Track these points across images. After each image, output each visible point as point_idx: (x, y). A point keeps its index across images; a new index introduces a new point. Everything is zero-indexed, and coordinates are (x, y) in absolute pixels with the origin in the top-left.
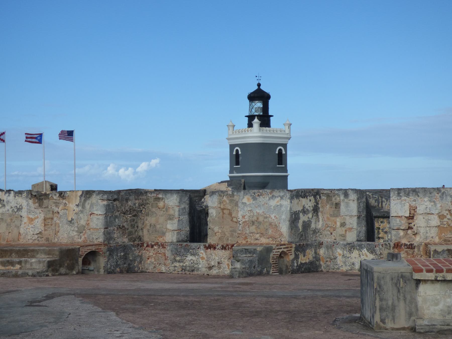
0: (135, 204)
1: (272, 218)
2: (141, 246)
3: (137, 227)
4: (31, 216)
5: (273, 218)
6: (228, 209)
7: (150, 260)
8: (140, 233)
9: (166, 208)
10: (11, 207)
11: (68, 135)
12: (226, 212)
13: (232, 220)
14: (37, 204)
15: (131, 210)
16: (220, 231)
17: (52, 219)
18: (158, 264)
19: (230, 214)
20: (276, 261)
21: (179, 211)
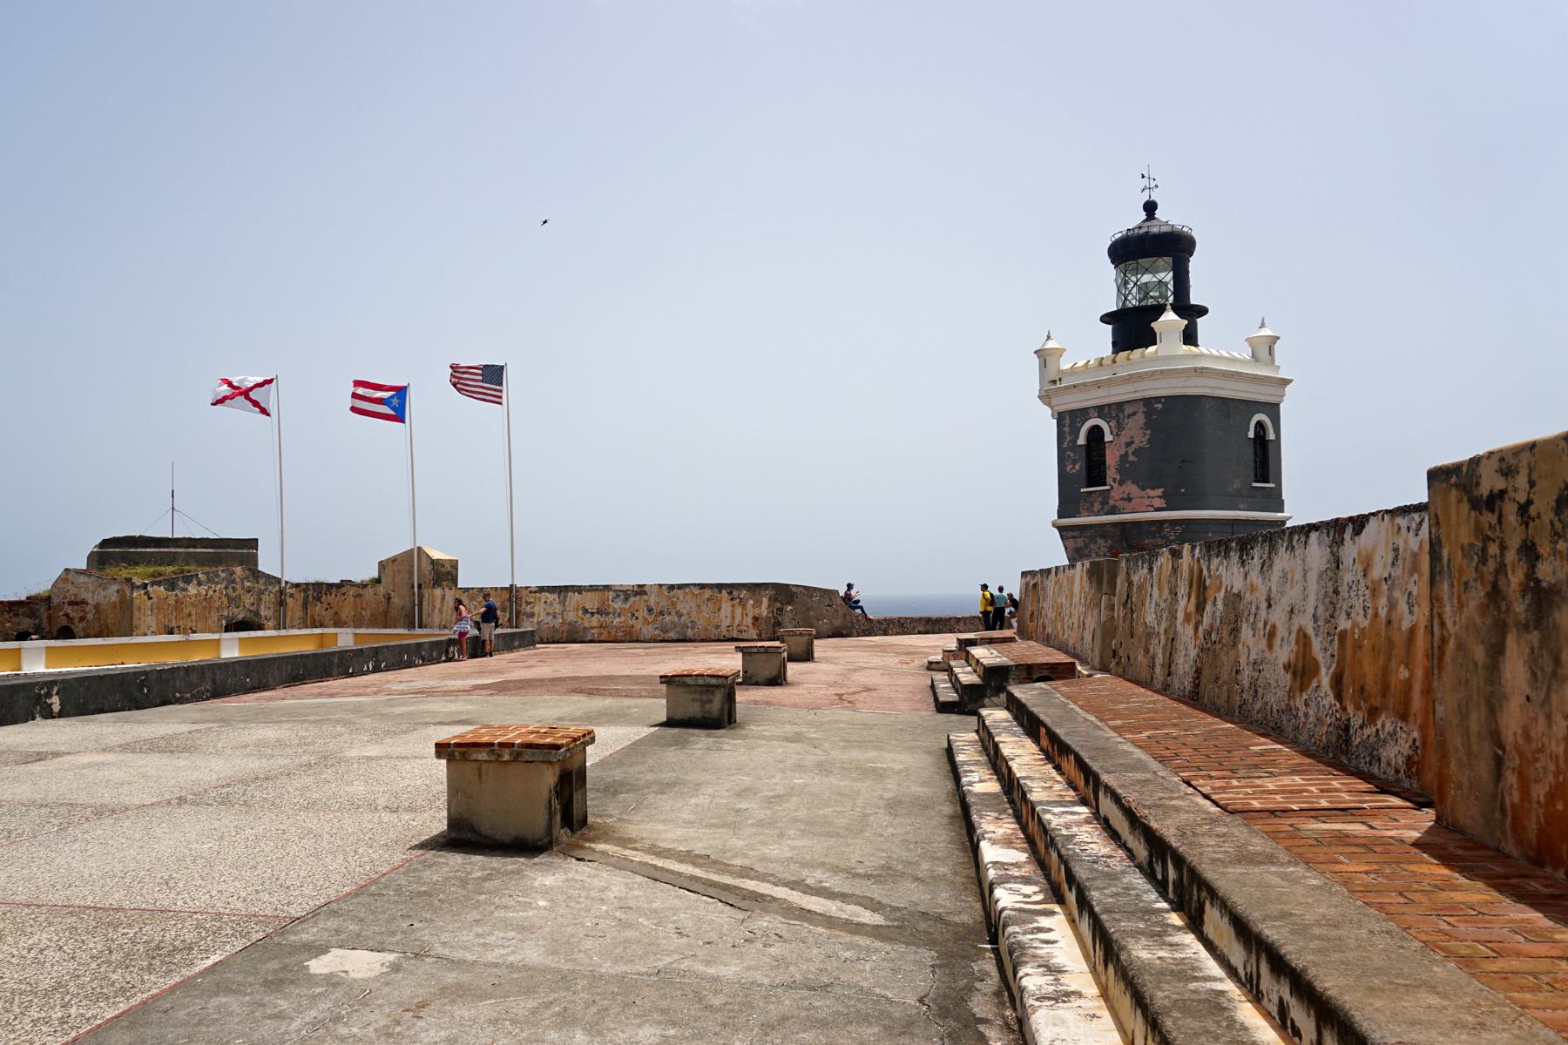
11: (485, 381)
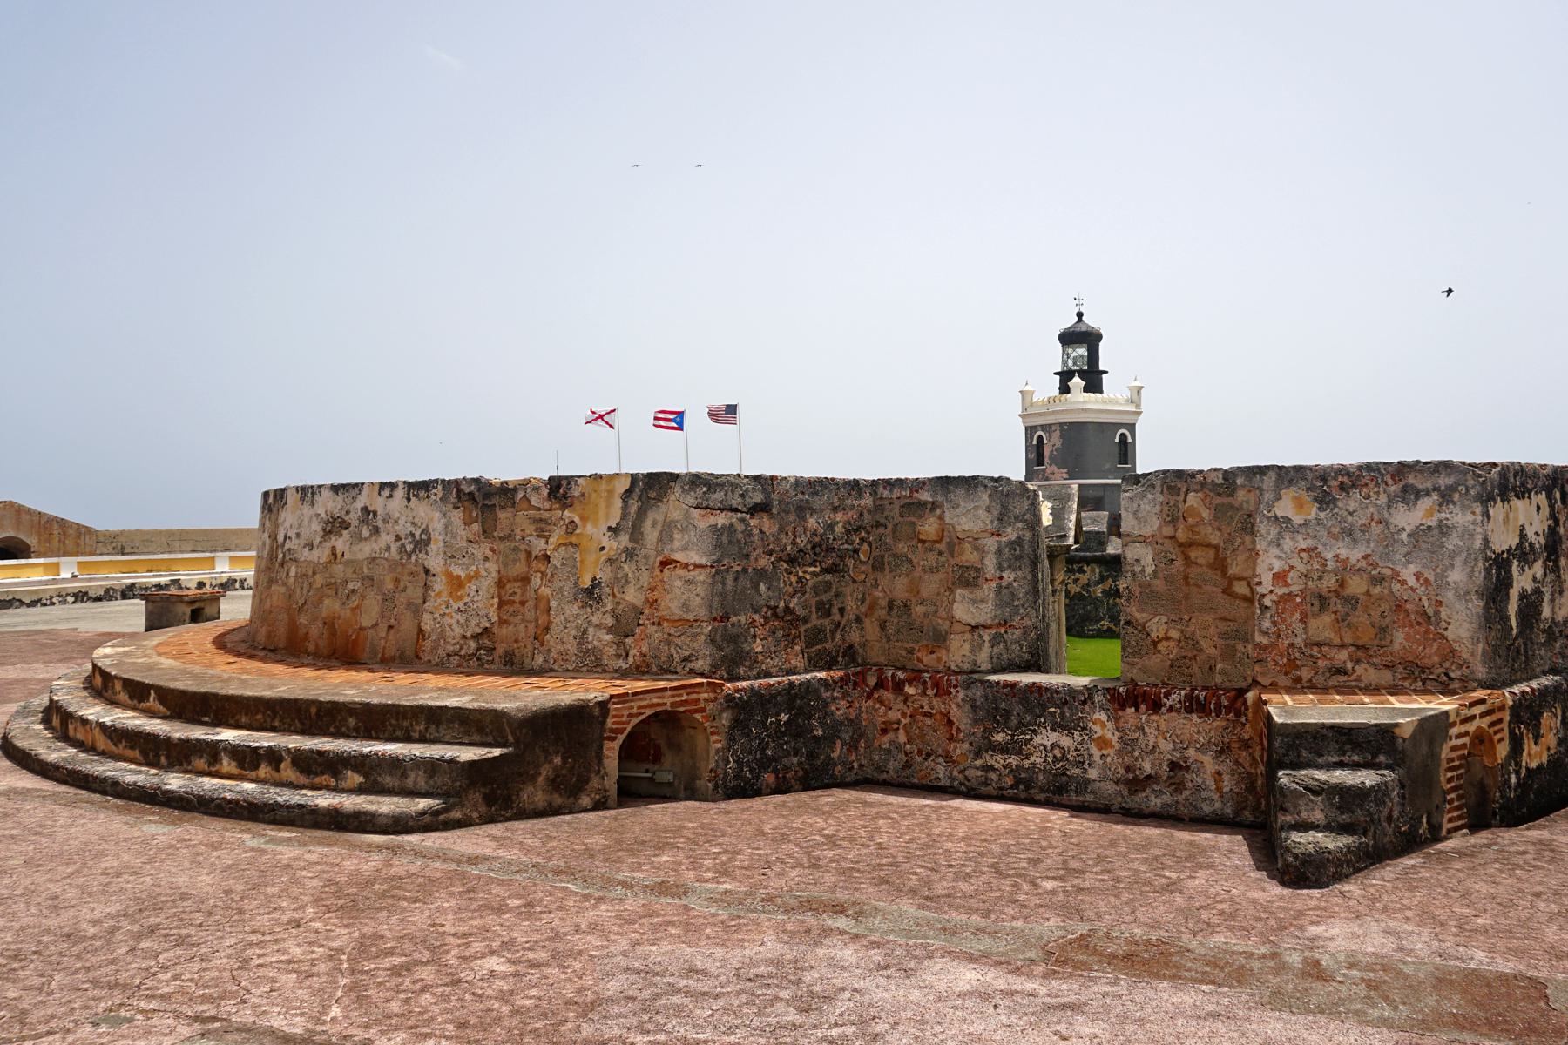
0: (831, 527)
1: (1404, 583)
2: (855, 685)
3: (842, 611)
4: (457, 571)
5: (1412, 582)
6: (1208, 545)
7: (891, 735)
8: (854, 637)
9: (950, 542)
10: (398, 538)
12: (1200, 556)
13: (1228, 591)
14: (476, 527)
15: (819, 547)
16: (1174, 634)
17: (525, 580)
18: (920, 752)
19: (1220, 565)
20: (1460, 777)
21: (999, 552)
